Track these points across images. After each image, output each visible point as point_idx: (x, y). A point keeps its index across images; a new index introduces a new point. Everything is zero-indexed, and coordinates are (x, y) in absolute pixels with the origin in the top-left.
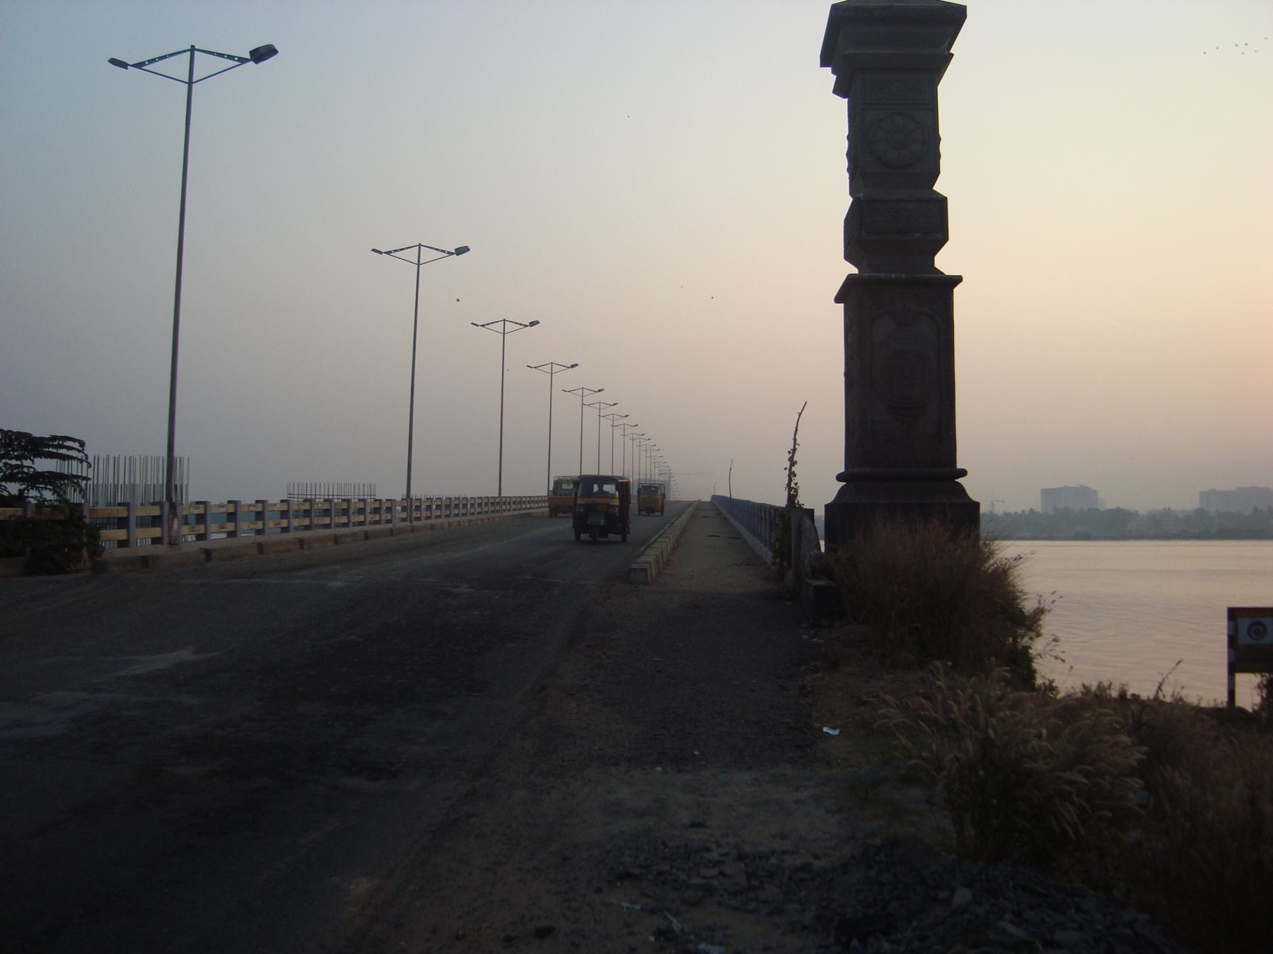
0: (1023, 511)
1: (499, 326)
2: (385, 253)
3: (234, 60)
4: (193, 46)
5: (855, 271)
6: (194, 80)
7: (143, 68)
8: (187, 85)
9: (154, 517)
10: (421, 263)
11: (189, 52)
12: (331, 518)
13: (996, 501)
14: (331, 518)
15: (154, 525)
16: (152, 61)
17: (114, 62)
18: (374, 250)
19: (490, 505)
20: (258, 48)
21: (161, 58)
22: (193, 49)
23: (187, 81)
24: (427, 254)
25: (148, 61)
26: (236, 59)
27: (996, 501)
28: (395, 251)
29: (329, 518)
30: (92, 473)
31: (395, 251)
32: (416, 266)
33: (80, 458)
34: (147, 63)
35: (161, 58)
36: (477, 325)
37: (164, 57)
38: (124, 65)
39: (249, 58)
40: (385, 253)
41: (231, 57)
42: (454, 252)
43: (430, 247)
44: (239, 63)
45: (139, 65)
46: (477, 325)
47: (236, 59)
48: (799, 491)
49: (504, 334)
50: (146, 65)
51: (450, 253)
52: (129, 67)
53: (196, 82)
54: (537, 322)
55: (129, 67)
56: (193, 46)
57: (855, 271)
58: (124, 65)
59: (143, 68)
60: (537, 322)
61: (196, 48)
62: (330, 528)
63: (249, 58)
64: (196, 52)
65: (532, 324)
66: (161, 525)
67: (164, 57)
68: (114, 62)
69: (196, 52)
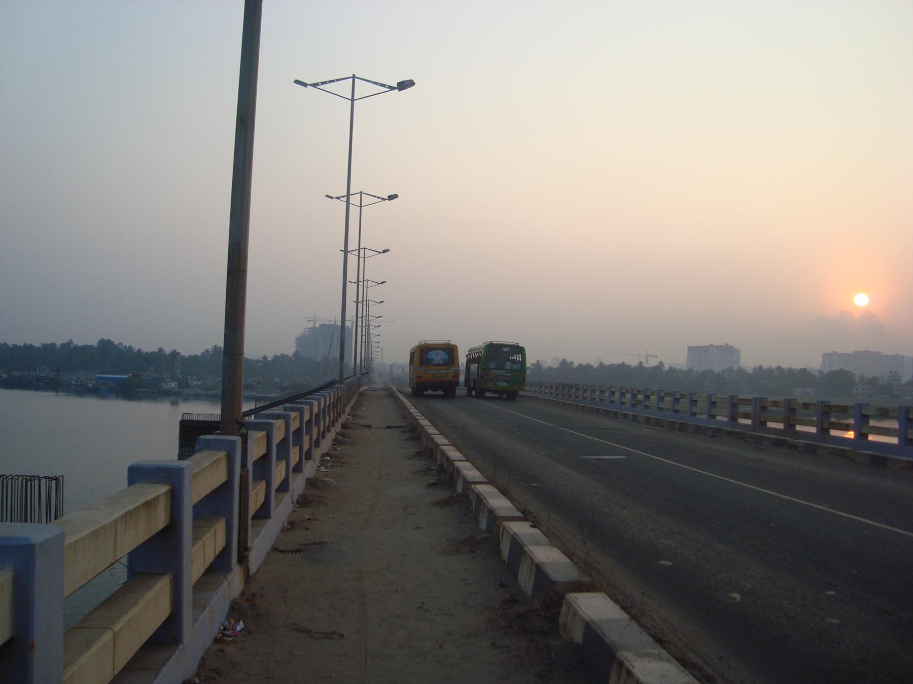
0: (265, 358)
1: (344, 88)
2: (310, 85)
3: (385, 87)
4: (354, 75)
5: (581, 643)
7: (317, 87)
11: (352, 79)
13: (649, 356)
17: (297, 82)
20: (403, 81)
21: (331, 82)
22: (354, 77)
23: (350, 98)
24: (362, 88)
25: (321, 83)
26: (387, 86)
27: (649, 356)
28: (323, 83)
31: (323, 83)
33: (357, 373)
34: (320, 84)
35: (331, 82)
37: (333, 81)
38: (305, 85)
39: (396, 87)
40: (310, 85)
45: (315, 85)
49: (353, 100)
50: (319, 85)
51: (392, 88)
52: (308, 86)
54: (411, 83)
55: (308, 86)
56: (354, 75)
57: (581, 643)
58: (305, 85)
59: (317, 87)
60: (411, 83)
61: (356, 76)
63: (396, 87)
64: (356, 79)
67: (333, 81)
68: (297, 82)
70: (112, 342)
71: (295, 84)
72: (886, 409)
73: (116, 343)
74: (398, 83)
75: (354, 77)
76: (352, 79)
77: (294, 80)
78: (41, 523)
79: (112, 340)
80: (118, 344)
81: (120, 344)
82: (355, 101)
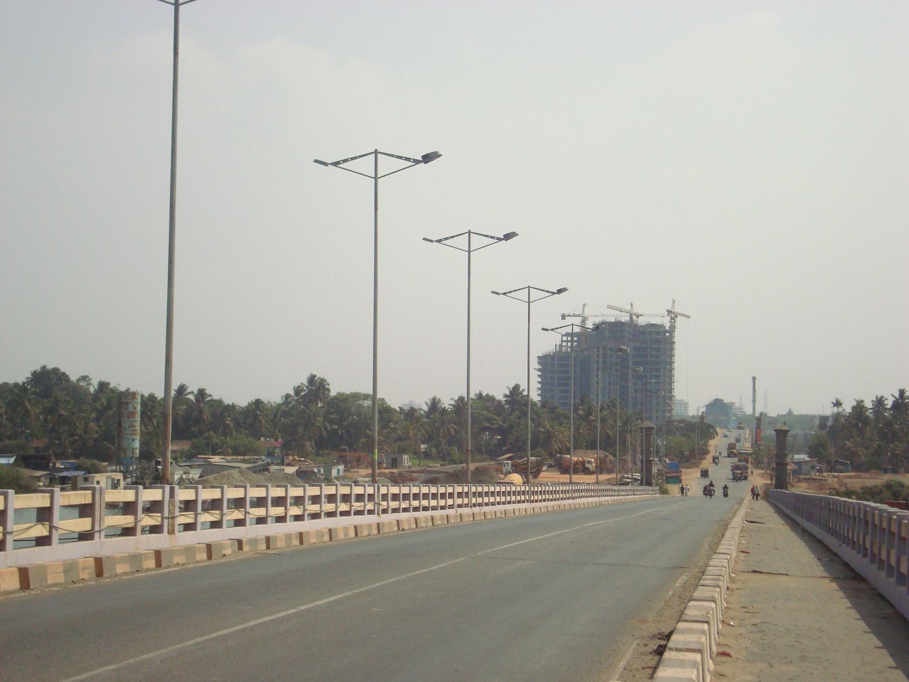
1: (462, 242)
2: (550, 330)
4: (469, 231)
6: (471, 250)
7: (338, 166)
8: (467, 253)
9: (213, 501)
10: (531, 301)
11: (374, 154)
12: (286, 509)
14: (286, 509)
15: (81, 515)
16: (447, 239)
18: (493, 292)
19: (323, 499)
22: (469, 232)
23: (467, 250)
28: (510, 292)
29: (283, 508)
30: (545, 476)
31: (510, 292)
32: (528, 303)
36: (431, 241)
38: (547, 330)
39: (421, 159)
40: (550, 330)
41: (408, 159)
42: (503, 237)
43: (536, 289)
44: (414, 164)
46: (431, 241)
47: (412, 160)
48: (723, 494)
49: (529, 302)
53: (379, 178)
55: (329, 165)
58: (547, 330)
59: (338, 166)
61: (379, 151)
62: (303, 520)
63: (421, 159)
64: (379, 155)
65: (508, 237)
66: (160, 511)
69: (379, 155)
70: (64, 374)
71: (315, 163)
72: (100, 558)
73: (74, 378)
74: (422, 156)
75: (469, 232)
76: (374, 154)
77: (314, 160)
78: (59, 543)
79: (62, 370)
80: (79, 380)
81: (84, 378)
82: (379, 179)
